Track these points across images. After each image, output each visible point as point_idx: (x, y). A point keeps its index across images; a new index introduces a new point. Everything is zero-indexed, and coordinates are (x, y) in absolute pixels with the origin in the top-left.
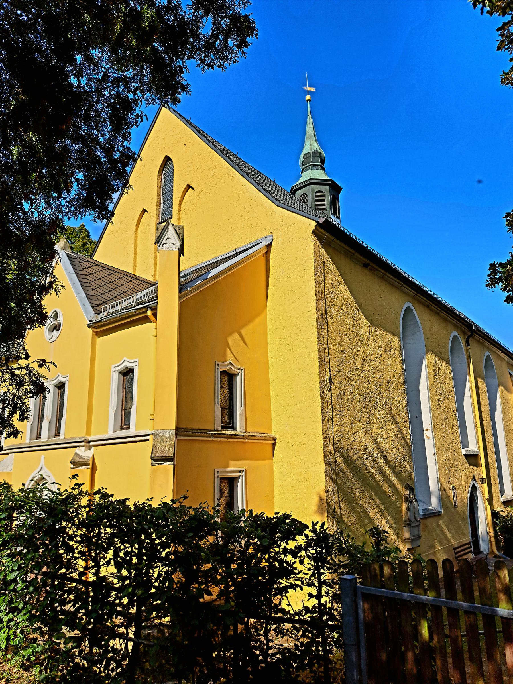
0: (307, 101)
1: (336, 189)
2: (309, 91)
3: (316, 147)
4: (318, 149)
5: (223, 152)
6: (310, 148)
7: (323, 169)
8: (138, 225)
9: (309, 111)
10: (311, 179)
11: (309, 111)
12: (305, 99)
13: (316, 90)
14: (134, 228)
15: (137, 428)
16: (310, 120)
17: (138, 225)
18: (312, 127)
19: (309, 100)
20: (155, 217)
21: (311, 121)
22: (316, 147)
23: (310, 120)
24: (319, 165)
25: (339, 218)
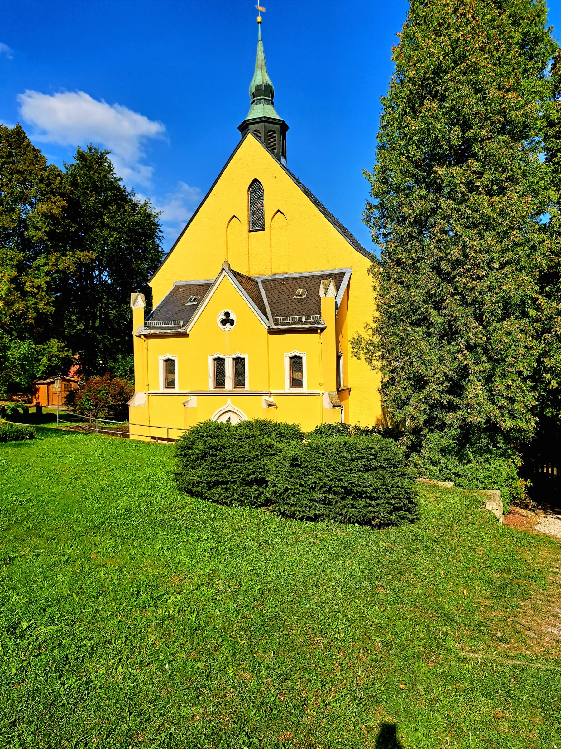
0: (259, 23)
1: (284, 127)
2: (261, 12)
3: (267, 80)
4: (270, 83)
5: (297, 181)
6: (263, 80)
7: (273, 104)
8: (227, 227)
9: (260, 35)
10: (265, 117)
11: (260, 35)
12: (256, 20)
13: (266, 10)
14: (226, 228)
15: (308, 387)
16: (260, 47)
17: (227, 227)
18: (263, 55)
19: (260, 23)
20: (247, 226)
21: (262, 48)
22: (267, 80)
23: (260, 47)
24: (270, 100)
25: (286, 158)
